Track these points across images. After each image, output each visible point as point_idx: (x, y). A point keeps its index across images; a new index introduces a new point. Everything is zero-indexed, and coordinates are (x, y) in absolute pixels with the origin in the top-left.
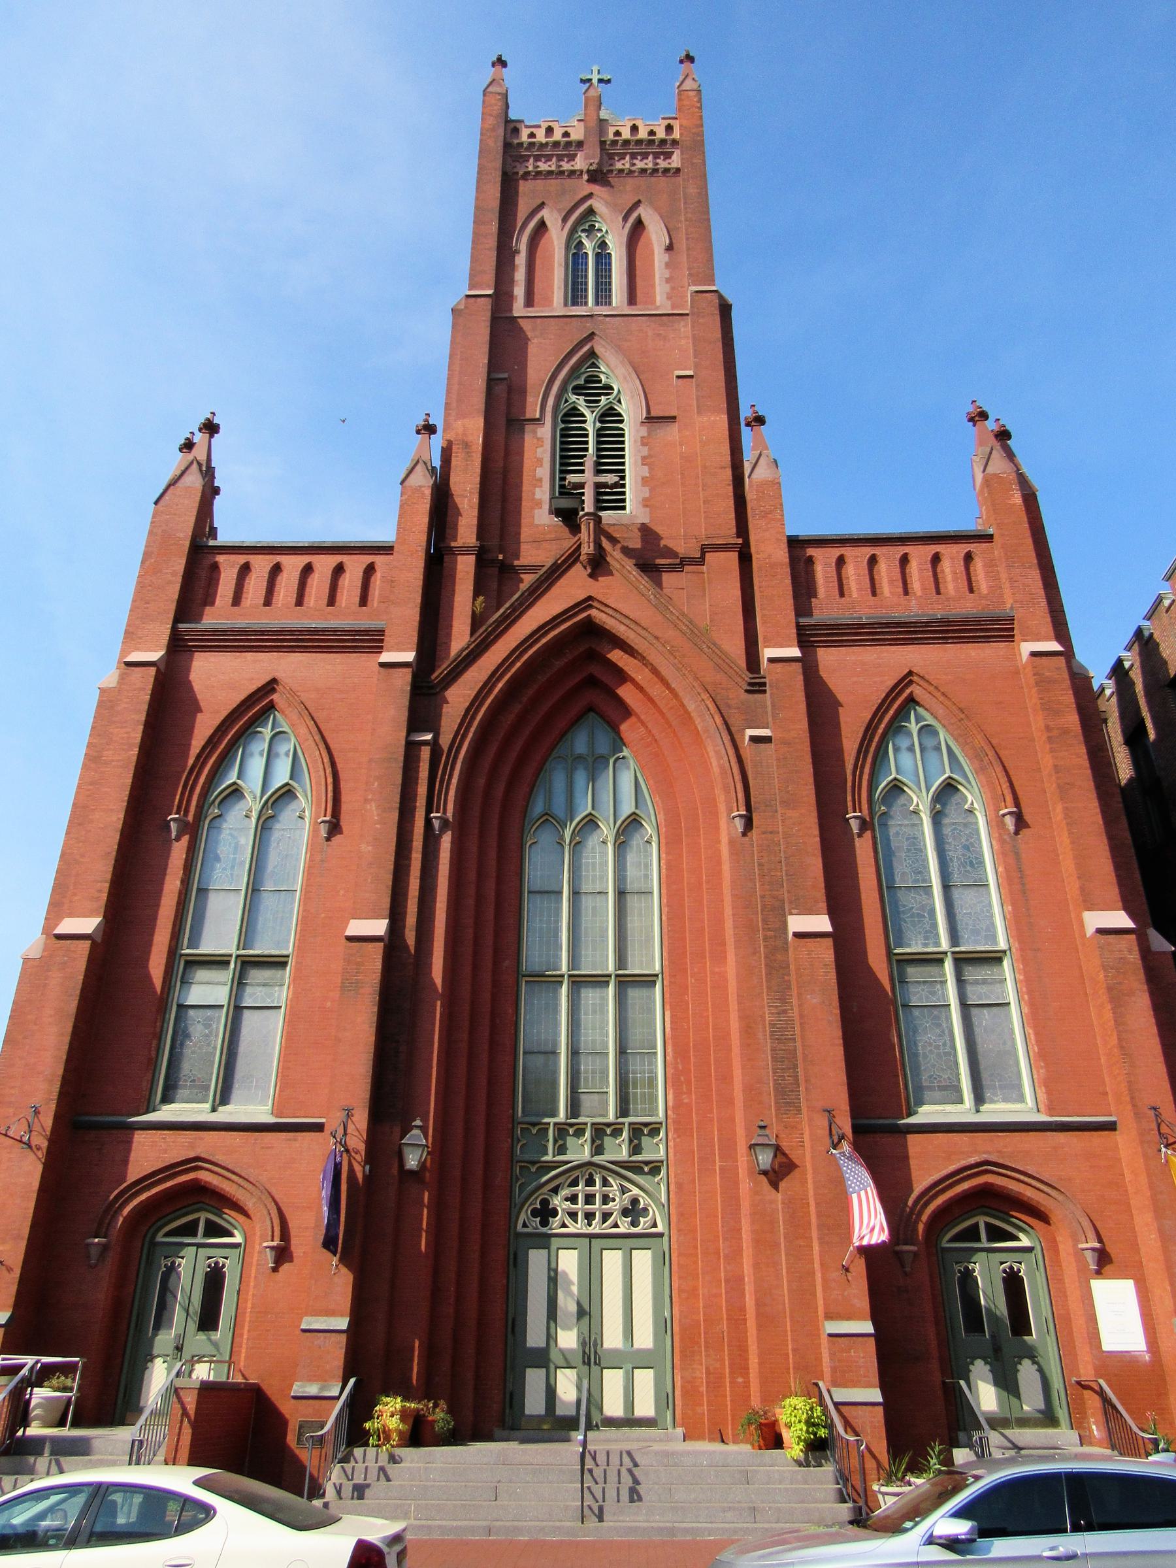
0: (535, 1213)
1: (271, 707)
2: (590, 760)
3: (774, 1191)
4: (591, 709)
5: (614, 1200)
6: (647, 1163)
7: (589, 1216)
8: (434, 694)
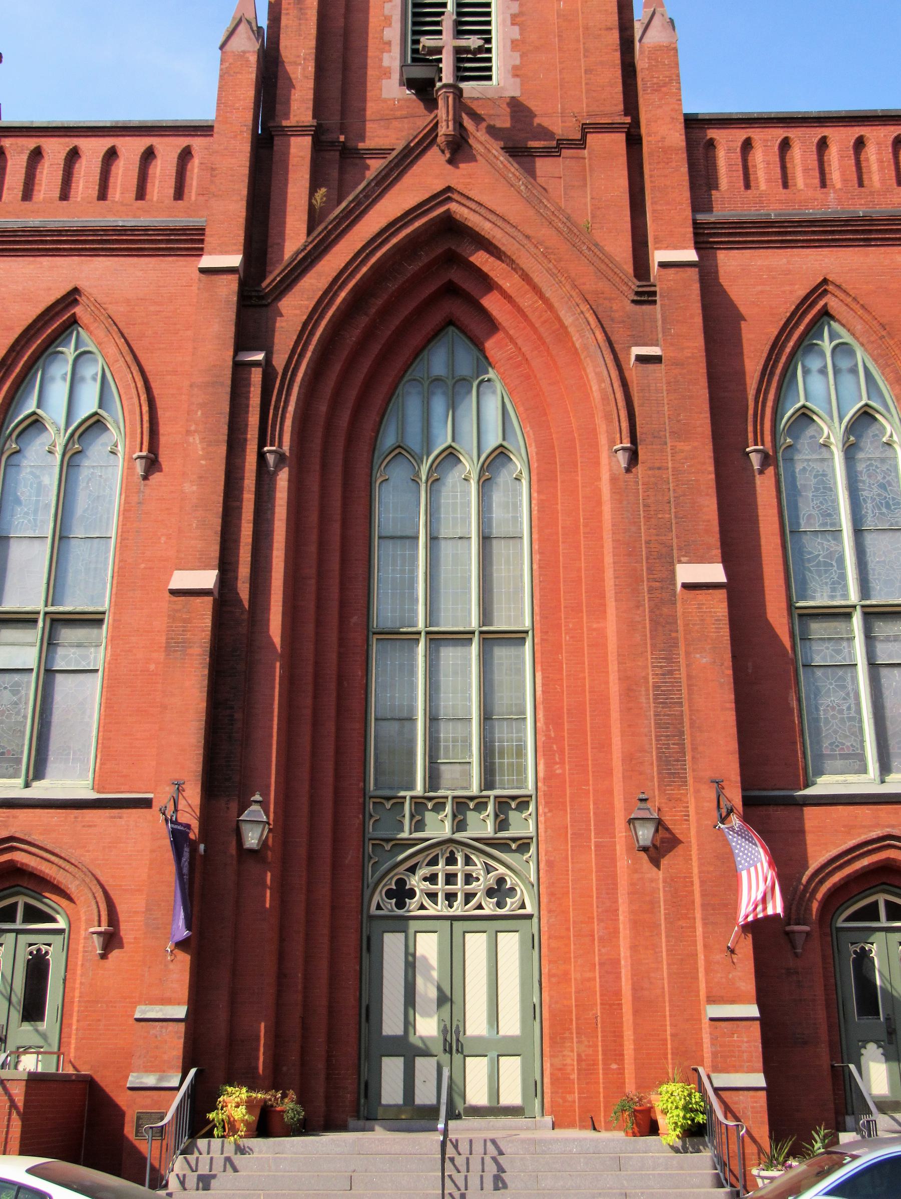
0: (390, 894)
1: (74, 321)
3: (655, 869)
4: (450, 322)
5: (478, 879)
6: (514, 840)
7: (450, 897)
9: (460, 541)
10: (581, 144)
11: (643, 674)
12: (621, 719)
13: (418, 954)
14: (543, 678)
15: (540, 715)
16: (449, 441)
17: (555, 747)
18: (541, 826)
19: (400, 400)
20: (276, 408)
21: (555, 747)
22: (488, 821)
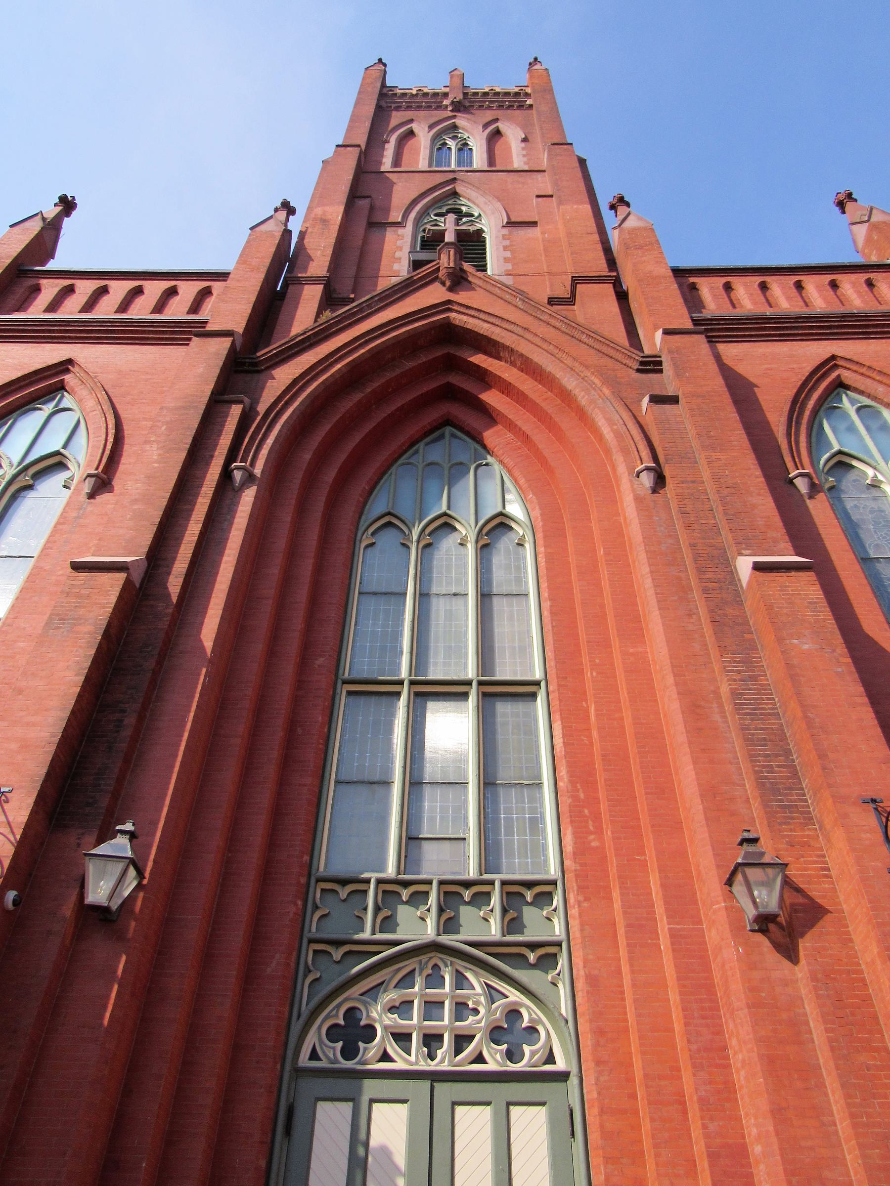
0: (333, 1033)
1: (61, 387)
2: (446, 466)
3: (786, 963)
4: (447, 422)
5: (476, 1011)
6: (533, 946)
7: (432, 1040)
8: (259, 372)
9: (454, 599)
10: (576, 281)
11: (712, 688)
12: (689, 742)
13: (373, 1143)
14: (563, 727)
15: (563, 771)
16: (444, 508)
17: (586, 811)
18: (574, 924)
19: (393, 482)
20: (253, 438)
21: (586, 811)
22: (492, 921)
